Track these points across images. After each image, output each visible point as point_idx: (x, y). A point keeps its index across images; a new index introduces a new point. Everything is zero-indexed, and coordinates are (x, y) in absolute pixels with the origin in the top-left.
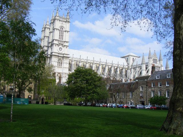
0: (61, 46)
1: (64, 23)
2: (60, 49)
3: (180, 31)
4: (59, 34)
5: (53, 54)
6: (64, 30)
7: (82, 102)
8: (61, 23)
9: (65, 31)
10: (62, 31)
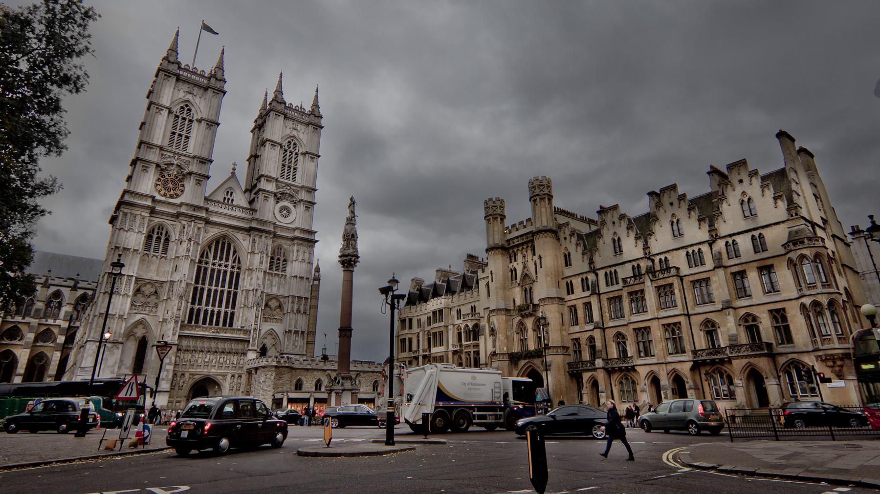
1: (300, 127)
2: (285, 212)
3: (863, 231)
4: (281, 163)
7: (224, 442)
8: (187, 90)
9: (304, 154)
10: (288, 153)
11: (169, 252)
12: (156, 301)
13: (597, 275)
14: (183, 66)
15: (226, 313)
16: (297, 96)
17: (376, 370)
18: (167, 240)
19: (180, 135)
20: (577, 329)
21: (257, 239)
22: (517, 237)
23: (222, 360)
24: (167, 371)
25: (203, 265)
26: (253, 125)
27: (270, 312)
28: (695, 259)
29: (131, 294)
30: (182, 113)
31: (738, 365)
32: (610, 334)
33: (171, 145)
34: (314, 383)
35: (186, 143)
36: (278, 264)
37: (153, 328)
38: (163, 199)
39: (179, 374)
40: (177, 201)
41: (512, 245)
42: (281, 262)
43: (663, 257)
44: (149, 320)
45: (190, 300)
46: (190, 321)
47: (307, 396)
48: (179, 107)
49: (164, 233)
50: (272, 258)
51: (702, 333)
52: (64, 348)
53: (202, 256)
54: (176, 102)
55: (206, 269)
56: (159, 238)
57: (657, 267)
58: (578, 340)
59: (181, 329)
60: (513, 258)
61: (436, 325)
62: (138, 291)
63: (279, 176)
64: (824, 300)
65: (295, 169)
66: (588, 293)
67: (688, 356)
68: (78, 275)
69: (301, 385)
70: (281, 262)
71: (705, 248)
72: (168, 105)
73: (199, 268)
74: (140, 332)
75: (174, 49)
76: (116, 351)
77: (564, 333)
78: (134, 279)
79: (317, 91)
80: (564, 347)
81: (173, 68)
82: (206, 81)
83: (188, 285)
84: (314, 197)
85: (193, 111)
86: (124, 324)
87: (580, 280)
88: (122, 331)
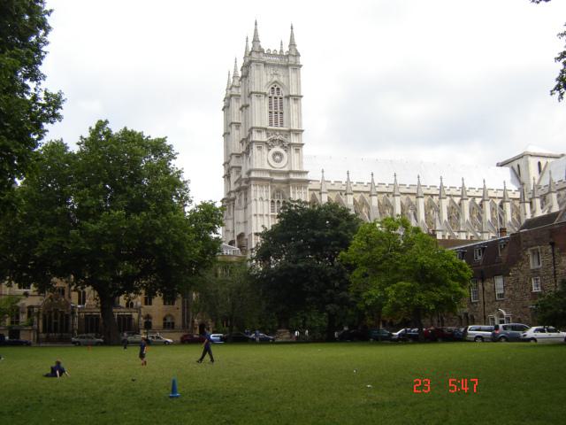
0: (278, 149)
2: (278, 157)
5: (253, 175)
6: (284, 93)
10: (273, 100)
16: (271, 43)
79: (256, 24)
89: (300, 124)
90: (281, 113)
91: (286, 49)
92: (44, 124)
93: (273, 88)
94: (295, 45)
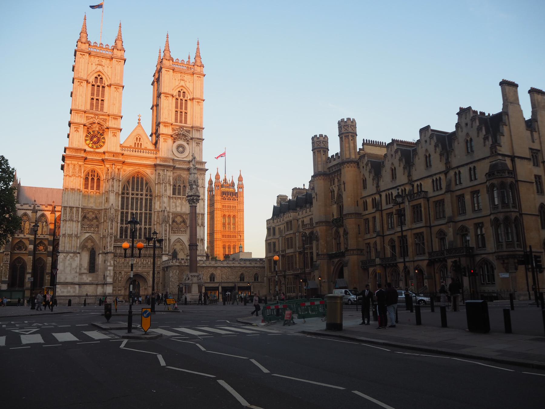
1: (105, 62)
2: (181, 149)
8: (97, 63)
10: (179, 101)
11: (101, 188)
12: (97, 223)
13: (381, 196)
14: (92, 45)
15: (145, 228)
16: (181, 53)
17: (256, 265)
18: (99, 180)
19: (97, 100)
20: (368, 236)
21: (161, 172)
22: (334, 166)
23: (145, 261)
24: (110, 270)
25: (126, 196)
26: (153, 79)
27: (177, 226)
28: (437, 184)
29: (80, 219)
30: (96, 82)
31: (450, 262)
32: (387, 239)
33: (92, 108)
34: (208, 276)
35: (102, 104)
36: (179, 190)
37: (98, 242)
38: (92, 150)
39: (118, 272)
40: (101, 150)
41: (332, 171)
42: (182, 188)
43: (418, 183)
44: (94, 237)
45: (119, 221)
46: (121, 237)
47: (217, 285)
48: (93, 77)
49: (96, 175)
50: (174, 186)
51: (437, 239)
52: (53, 254)
53: (124, 189)
54: (91, 75)
55: (128, 198)
56: (93, 179)
57: (416, 191)
58: (369, 244)
59: (114, 242)
60: (332, 182)
61: (289, 233)
62: (84, 217)
63: (173, 120)
64: (501, 217)
65: (186, 113)
66: (375, 210)
67: (426, 257)
68: (54, 202)
69: (214, 278)
70: (182, 188)
71: (443, 177)
72: (85, 78)
73: (123, 198)
74: (90, 245)
75: (84, 32)
76: (76, 259)
77: (360, 239)
78: (80, 209)
79: (198, 44)
80: (358, 249)
81: (85, 47)
82: (110, 53)
83: (116, 211)
84: (201, 135)
85: (104, 79)
86: (78, 240)
87: (371, 199)
88: (78, 246)
89: (201, 123)
90: (102, 100)
91: (192, 60)
92: (330, 155)
93: (179, 92)
94: (200, 57)
